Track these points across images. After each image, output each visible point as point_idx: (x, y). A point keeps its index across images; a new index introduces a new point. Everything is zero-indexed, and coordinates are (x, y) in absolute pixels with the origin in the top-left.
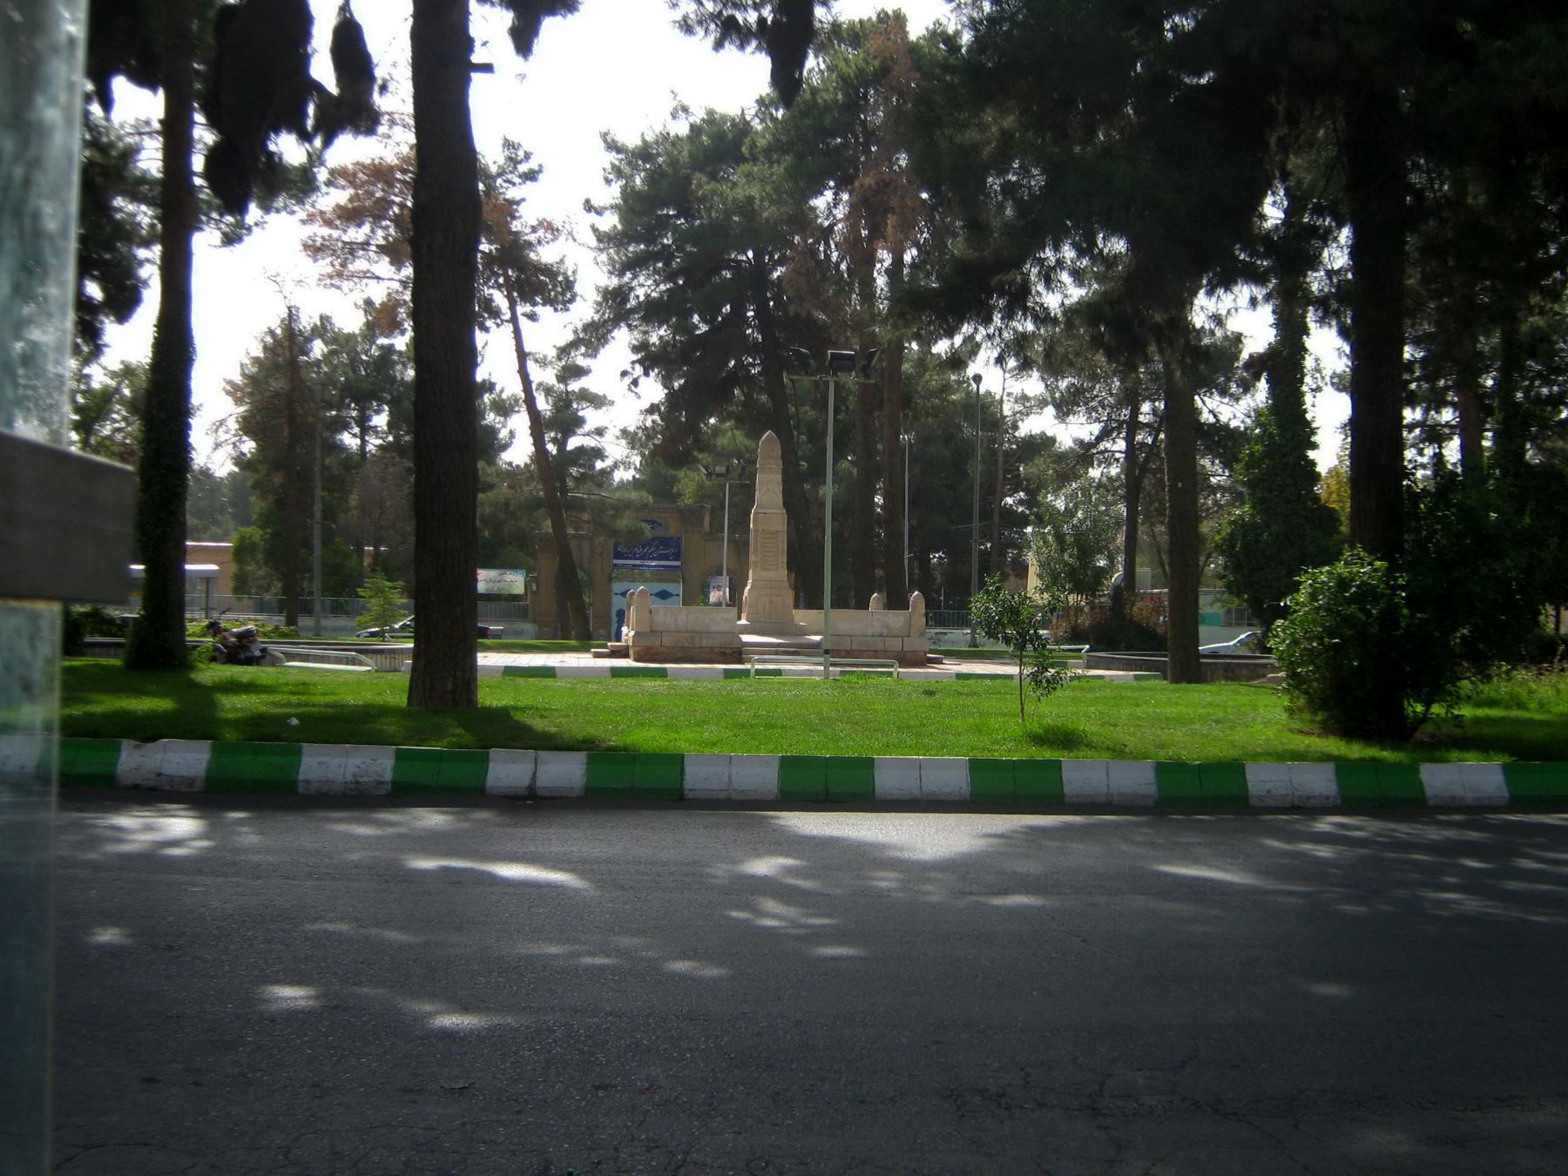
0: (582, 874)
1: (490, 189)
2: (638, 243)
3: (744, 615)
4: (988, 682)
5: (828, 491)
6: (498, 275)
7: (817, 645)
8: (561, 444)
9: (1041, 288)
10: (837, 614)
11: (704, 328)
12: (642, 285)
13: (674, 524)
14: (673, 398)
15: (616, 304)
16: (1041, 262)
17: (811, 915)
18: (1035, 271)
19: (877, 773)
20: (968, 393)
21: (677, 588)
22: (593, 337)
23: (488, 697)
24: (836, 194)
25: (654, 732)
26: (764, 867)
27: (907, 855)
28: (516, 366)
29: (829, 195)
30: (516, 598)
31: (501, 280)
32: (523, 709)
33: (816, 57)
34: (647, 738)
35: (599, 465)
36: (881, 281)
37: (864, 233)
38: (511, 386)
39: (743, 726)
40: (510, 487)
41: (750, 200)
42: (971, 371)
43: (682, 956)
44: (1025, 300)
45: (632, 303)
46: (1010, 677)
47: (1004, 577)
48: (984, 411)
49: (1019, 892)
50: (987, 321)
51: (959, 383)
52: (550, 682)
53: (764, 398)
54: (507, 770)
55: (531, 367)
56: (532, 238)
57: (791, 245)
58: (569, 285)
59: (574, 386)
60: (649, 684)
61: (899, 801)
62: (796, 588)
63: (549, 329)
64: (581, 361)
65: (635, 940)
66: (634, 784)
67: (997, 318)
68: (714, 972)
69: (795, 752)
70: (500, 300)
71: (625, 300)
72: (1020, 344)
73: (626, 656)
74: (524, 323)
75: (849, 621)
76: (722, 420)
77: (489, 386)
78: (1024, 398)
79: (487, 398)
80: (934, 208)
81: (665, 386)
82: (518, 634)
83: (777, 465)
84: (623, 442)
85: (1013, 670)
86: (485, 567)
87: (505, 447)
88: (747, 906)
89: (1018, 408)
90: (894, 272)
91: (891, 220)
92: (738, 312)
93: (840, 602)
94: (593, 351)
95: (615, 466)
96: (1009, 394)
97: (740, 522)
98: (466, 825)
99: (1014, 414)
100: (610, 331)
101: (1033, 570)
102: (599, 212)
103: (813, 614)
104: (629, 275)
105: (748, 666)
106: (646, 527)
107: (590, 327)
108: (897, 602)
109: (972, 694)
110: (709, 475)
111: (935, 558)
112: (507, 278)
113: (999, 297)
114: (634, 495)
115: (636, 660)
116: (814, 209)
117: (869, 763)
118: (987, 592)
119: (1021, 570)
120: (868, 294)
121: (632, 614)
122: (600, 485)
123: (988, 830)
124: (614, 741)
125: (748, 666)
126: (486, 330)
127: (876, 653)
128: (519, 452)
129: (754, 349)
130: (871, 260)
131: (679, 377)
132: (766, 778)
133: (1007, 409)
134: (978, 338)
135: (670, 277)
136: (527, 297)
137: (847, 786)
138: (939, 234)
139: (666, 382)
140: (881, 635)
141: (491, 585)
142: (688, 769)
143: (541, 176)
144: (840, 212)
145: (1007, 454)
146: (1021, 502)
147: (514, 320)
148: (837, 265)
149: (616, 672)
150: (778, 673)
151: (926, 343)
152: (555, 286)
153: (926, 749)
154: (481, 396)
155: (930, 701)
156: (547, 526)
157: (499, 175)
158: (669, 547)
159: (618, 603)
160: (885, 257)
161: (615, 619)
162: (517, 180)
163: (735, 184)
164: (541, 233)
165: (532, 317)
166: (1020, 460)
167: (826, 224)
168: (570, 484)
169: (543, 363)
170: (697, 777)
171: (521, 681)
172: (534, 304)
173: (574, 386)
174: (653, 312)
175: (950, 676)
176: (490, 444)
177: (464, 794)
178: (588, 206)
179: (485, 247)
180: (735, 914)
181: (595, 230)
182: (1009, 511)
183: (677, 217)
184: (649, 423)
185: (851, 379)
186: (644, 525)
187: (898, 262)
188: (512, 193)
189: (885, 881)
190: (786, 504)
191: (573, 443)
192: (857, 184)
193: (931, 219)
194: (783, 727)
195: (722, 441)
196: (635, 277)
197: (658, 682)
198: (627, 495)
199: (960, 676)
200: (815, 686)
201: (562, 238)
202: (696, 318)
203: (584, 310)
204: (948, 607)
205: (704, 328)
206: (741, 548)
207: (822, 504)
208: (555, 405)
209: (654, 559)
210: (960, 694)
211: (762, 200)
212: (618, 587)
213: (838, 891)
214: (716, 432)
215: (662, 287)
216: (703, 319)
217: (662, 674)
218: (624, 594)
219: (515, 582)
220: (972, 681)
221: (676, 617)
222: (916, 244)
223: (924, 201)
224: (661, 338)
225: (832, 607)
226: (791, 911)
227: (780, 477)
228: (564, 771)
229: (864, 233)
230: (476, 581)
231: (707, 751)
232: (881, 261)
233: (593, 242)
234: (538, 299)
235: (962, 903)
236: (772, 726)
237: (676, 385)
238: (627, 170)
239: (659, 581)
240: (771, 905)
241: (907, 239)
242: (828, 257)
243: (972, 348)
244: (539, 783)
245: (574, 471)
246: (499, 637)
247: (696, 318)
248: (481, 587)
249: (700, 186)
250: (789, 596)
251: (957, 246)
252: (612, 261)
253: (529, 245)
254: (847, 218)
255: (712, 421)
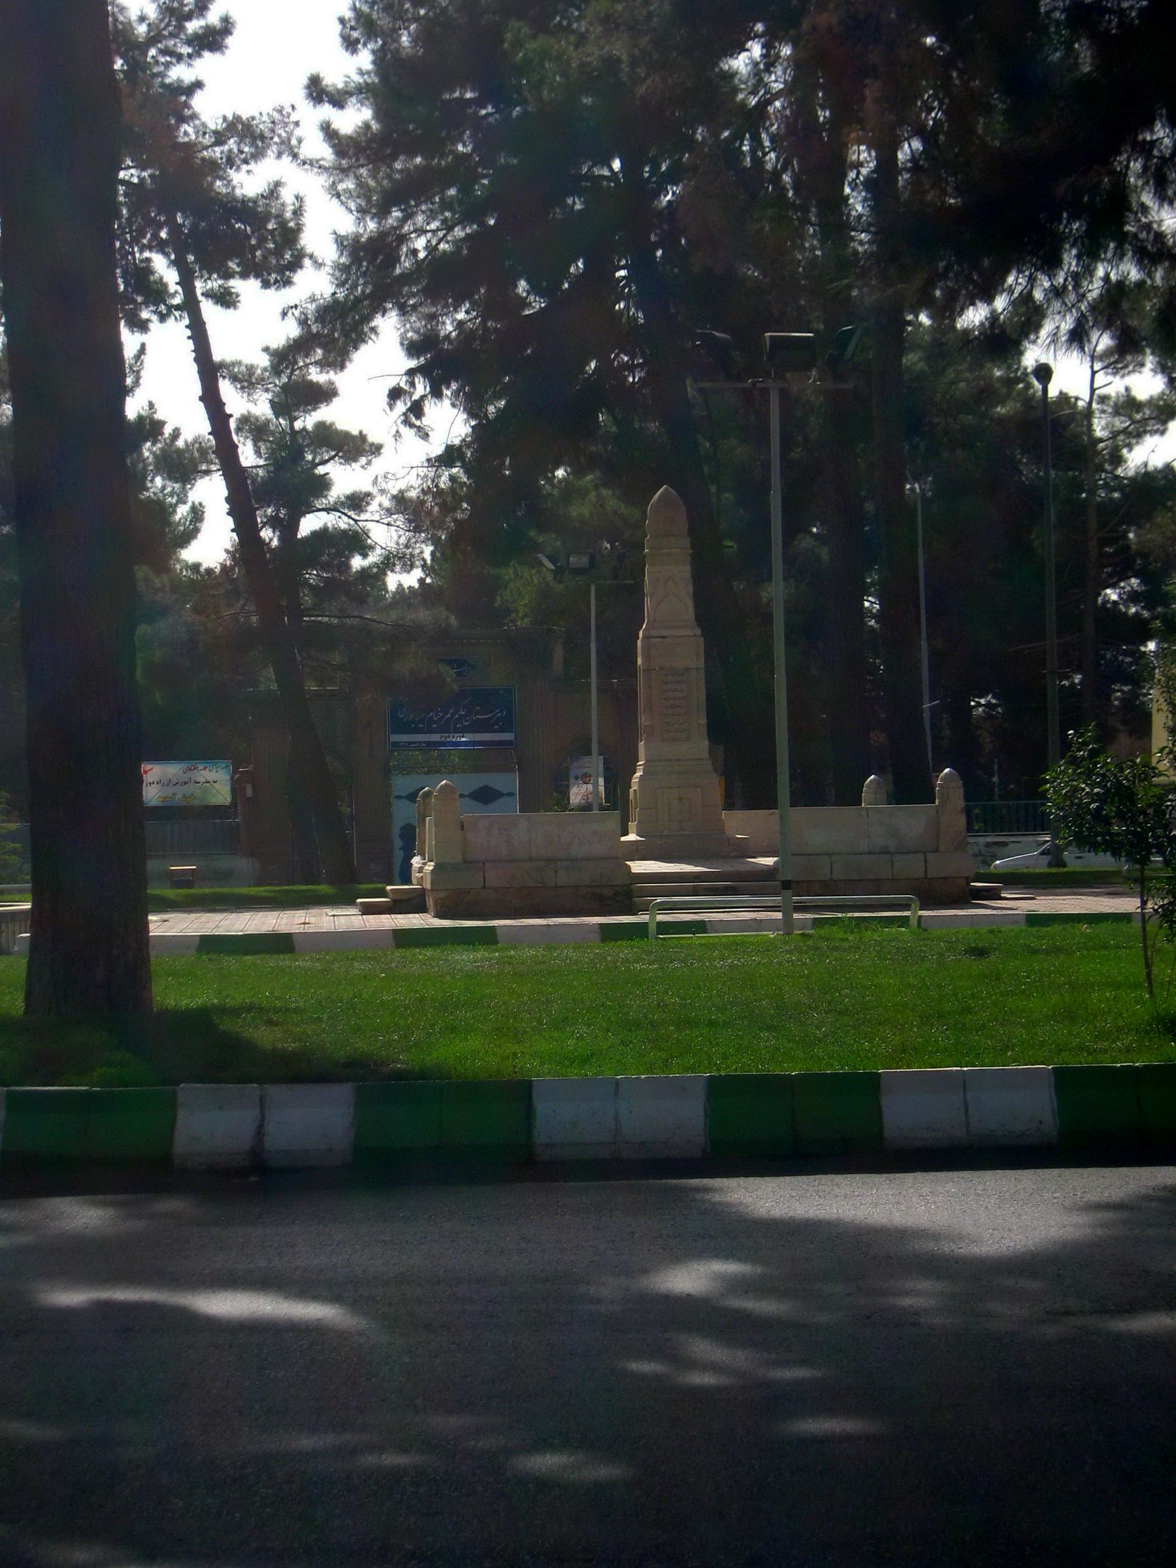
0: (355, 1304)
1: (137, 67)
2: (412, 155)
3: (632, 825)
4: (1084, 927)
5: (777, 592)
6: (160, 227)
7: (768, 874)
8: (288, 527)
9: (1147, 198)
10: (802, 815)
11: (537, 304)
12: (421, 232)
13: (493, 655)
14: (486, 436)
15: (374, 273)
16: (1146, 149)
17: (776, 1364)
18: (1136, 166)
19: (885, 1101)
20: (1028, 401)
21: (509, 782)
22: (335, 331)
23: (170, 993)
24: (767, 46)
25: (474, 1042)
26: (688, 1279)
27: (946, 1248)
28: (197, 389)
29: (756, 49)
30: (218, 811)
31: (163, 234)
32: (236, 1012)
33: (920, 360)
34: (470, 1052)
35: (357, 562)
36: (858, 205)
37: (823, 115)
38: (188, 422)
39: (638, 1025)
40: (196, 610)
41: (611, 64)
42: (1031, 357)
43: (542, 1445)
44: (1122, 222)
45: (406, 264)
46: (1125, 917)
47: (1106, 737)
48: (1057, 430)
49: (1156, 1309)
50: (1051, 263)
51: (1010, 382)
52: (284, 961)
53: (653, 426)
54: (210, 1122)
55: (226, 388)
56: (217, 152)
57: (689, 143)
58: (289, 236)
59: (307, 421)
60: (465, 957)
61: (258, 903)
62: (728, 774)
63: (254, 322)
64: (316, 376)
65: (454, 1421)
66: (439, 1136)
67: (1070, 260)
68: (604, 1472)
69: (733, 1069)
70: (163, 268)
71: (395, 259)
72: (1114, 307)
73: (421, 909)
74: (209, 310)
75: (824, 829)
76: (578, 471)
77: (150, 427)
78: (1128, 404)
79: (148, 450)
80: (948, 63)
81: (471, 414)
82: (225, 876)
83: (681, 545)
84: (400, 519)
85: (1129, 904)
86: (162, 755)
87: (188, 536)
88: (655, 1353)
89: (1120, 423)
90: (879, 186)
91: (872, 90)
92: (600, 272)
93: (809, 793)
94: (337, 359)
95: (387, 563)
96: (1103, 399)
97: (619, 658)
98: (140, 1225)
99: (1115, 435)
100: (369, 318)
101: (1160, 720)
102: (338, 100)
103: (760, 816)
104: (396, 214)
105: (643, 918)
106: (448, 673)
107: (330, 312)
108: (911, 788)
109: (1058, 950)
110: (559, 572)
111: (980, 704)
112: (175, 229)
113: (1073, 217)
114: (423, 615)
115: (440, 915)
116: (731, 75)
117: (872, 1084)
118: (1074, 762)
119: (1141, 723)
120: (836, 224)
121: (429, 831)
122: (361, 600)
123: (1093, 1197)
124: (404, 1061)
125: (643, 918)
126: (143, 326)
127: (877, 886)
128: (212, 545)
129: (630, 338)
130: (839, 167)
131: (498, 397)
132: (685, 1118)
133: (1099, 428)
134: (1038, 295)
135: (470, 212)
136: (215, 265)
137: (839, 1130)
138: (961, 111)
139: (473, 405)
140: (885, 851)
141: (170, 791)
142: (542, 1107)
143: (230, 41)
144: (776, 81)
145: (1107, 508)
146: (1133, 597)
147: (191, 306)
148: (776, 175)
149: (403, 938)
150: (701, 926)
151: (947, 311)
152: (262, 241)
153: (974, 1055)
154: (138, 448)
155: (981, 966)
156: (268, 680)
157: (152, 40)
158: (489, 708)
159: (402, 813)
160: (864, 156)
161: (398, 843)
162: (185, 50)
163: (582, 39)
164: (232, 143)
165: (226, 299)
166: (1131, 519)
167: (753, 101)
168: (308, 600)
169: (247, 381)
170: (558, 1120)
171: (230, 962)
172: (228, 275)
173: (307, 421)
174: (441, 280)
175: (1014, 919)
176: (166, 533)
177: (141, 1171)
178: (317, 91)
179: (129, 174)
180: (635, 1366)
181: (328, 131)
182: (1111, 612)
183: (480, 102)
184: (444, 481)
185: (811, 383)
186: (444, 668)
187: (887, 163)
188: (179, 73)
189: (920, 1296)
190: (701, 619)
191: (309, 524)
192: (805, 26)
193: (945, 85)
194: (711, 1024)
195: (579, 510)
196: (408, 216)
197: (481, 953)
198: (410, 616)
199: (1034, 920)
200: (768, 947)
201: (271, 153)
202: (522, 286)
203: (314, 284)
204: (1007, 802)
205: (537, 304)
206: (623, 704)
207: (767, 618)
208: (272, 457)
209: (464, 731)
210: (1035, 952)
211: (633, 64)
212: (401, 784)
213: (823, 1318)
214: (568, 491)
215: (458, 232)
216: (534, 289)
217: (488, 937)
218: (412, 797)
219: (215, 783)
220: (1056, 928)
221: (519, 833)
222: (920, 131)
223: (931, 50)
224: (460, 325)
225: (794, 804)
226: (740, 1358)
227: (685, 570)
228: (312, 1120)
229: (823, 115)
230: (140, 781)
231: (574, 1073)
232: (859, 165)
233: (324, 152)
234: (233, 265)
235: (1051, 1331)
236: (692, 1023)
237: (491, 409)
238: (384, 21)
239: (478, 770)
240: (703, 1348)
241: (902, 122)
242: (758, 163)
243: (1028, 318)
244: (270, 1143)
245: (312, 576)
246: (189, 884)
247: (522, 286)
248: (151, 794)
249: (518, 44)
250: (714, 787)
251: (992, 129)
252: (363, 190)
253: (213, 168)
254: (790, 90)
255: (560, 473)
